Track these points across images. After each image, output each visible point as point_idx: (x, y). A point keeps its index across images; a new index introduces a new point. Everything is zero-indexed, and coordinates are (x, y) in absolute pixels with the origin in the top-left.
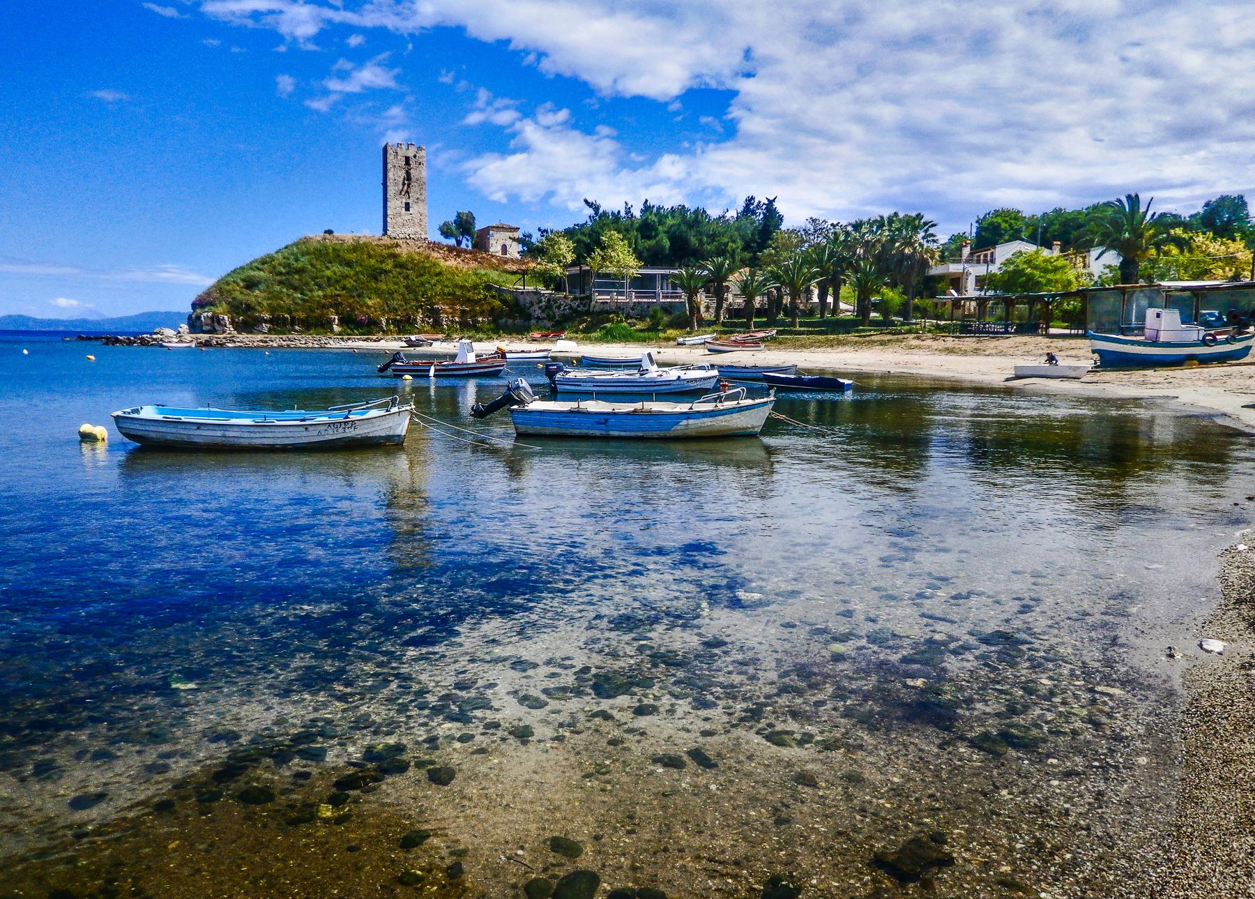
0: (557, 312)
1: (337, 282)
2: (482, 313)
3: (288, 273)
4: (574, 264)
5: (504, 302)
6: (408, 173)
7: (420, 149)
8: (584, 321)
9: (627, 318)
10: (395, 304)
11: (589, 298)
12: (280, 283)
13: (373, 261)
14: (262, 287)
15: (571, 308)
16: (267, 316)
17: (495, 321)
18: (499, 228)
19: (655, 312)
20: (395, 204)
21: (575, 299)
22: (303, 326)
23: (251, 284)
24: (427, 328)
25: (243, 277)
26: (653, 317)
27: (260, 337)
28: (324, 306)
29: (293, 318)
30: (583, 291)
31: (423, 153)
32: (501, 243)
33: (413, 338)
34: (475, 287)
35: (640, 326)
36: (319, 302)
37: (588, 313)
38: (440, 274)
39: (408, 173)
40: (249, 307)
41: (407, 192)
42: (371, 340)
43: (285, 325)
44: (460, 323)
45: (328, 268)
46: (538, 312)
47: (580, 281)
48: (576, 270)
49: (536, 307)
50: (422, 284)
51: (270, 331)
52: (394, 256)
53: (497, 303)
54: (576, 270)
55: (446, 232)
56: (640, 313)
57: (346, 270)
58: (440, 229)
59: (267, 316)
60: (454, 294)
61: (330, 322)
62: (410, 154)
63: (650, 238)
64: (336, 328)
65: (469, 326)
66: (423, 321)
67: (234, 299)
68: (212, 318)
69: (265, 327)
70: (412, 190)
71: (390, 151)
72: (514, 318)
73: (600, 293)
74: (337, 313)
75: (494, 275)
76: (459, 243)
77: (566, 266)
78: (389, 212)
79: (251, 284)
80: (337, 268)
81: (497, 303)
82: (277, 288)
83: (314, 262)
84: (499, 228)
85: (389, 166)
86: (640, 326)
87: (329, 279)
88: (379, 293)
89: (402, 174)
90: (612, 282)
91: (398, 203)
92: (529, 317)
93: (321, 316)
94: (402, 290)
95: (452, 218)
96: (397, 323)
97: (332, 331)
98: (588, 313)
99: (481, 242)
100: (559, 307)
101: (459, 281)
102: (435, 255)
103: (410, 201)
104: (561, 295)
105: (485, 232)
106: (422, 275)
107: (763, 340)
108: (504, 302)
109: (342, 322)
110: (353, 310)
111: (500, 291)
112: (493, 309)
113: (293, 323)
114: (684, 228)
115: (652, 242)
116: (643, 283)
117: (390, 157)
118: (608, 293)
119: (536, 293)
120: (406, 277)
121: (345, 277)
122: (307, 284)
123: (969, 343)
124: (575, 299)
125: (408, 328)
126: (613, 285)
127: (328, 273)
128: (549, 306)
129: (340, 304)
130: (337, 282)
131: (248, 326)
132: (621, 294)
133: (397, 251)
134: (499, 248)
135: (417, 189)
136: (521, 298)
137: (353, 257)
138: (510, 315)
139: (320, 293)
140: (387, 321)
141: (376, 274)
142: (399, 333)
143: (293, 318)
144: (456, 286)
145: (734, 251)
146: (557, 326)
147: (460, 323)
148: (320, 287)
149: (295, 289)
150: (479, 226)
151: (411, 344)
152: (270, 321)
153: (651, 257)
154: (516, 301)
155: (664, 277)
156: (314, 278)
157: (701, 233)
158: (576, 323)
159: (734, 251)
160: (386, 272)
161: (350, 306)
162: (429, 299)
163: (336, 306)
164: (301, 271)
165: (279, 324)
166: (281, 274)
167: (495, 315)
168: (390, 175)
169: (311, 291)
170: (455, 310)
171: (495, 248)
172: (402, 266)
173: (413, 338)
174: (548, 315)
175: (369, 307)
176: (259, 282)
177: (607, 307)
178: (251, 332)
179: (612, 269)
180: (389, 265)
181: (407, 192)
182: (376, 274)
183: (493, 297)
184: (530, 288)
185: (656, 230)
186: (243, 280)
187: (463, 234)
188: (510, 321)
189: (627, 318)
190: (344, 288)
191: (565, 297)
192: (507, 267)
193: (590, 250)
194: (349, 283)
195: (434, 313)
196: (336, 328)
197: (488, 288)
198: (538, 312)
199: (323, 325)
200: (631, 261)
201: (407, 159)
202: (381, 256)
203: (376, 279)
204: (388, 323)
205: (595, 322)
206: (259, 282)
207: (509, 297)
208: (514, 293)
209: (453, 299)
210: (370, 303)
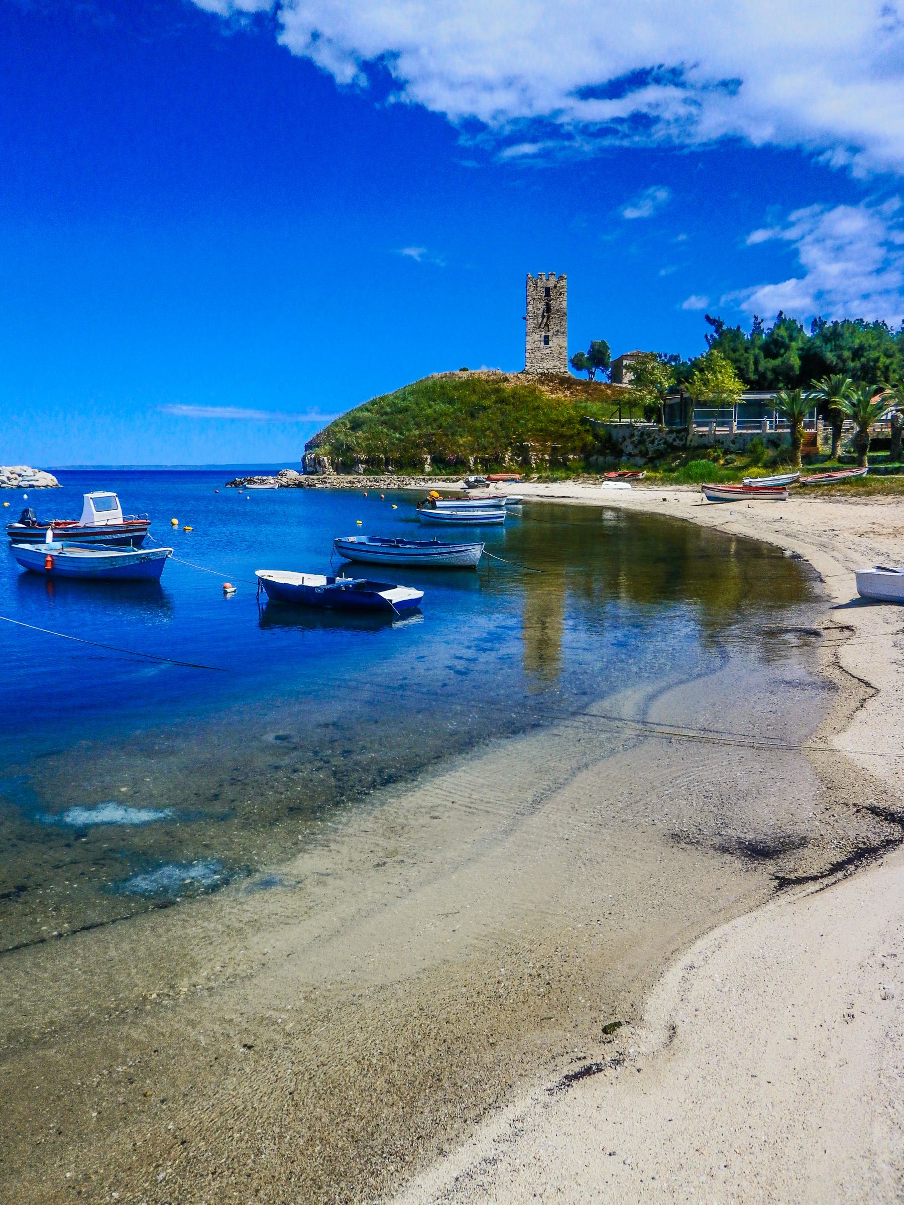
0: (651, 448)
2: (573, 450)
4: (673, 390)
5: (596, 436)
6: (548, 306)
7: (561, 278)
8: (678, 458)
11: (686, 430)
12: (384, 423)
14: (365, 428)
15: (665, 443)
16: (363, 457)
17: (586, 459)
21: (671, 432)
22: (396, 466)
23: (356, 425)
28: (418, 446)
31: (563, 283)
33: (472, 479)
34: (570, 421)
36: (414, 442)
37: (684, 448)
39: (548, 306)
40: (349, 448)
41: (547, 325)
44: (550, 461)
45: (430, 407)
46: (630, 449)
49: (628, 441)
52: (497, 391)
55: (577, 363)
58: (571, 361)
59: (363, 457)
61: (422, 462)
62: (551, 284)
63: (775, 357)
66: (511, 460)
67: (337, 440)
68: (314, 459)
72: (605, 455)
73: (698, 426)
74: (430, 453)
79: (356, 425)
80: (440, 407)
87: (428, 417)
88: (472, 431)
89: (541, 306)
90: (720, 411)
91: (537, 337)
94: (496, 427)
97: (422, 472)
98: (684, 448)
100: (653, 442)
103: (550, 334)
107: (844, 481)
111: (594, 425)
112: (585, 445)
113: (387, 464)
114: (818, 343)
115: (778, 362)
123: (863, 499)
124: (671, 432)
125: (495, 467)
126: (710, 415)
127: (429, 411)
128: (641, 442)
129: (435, 443)
130: (435, 420)
131: (345, 468)
136: (614, 433)
138: (601, 452)
139: (417, 432)
140: (476, 459)
143: (387, 459)
145: (887, 368)
147: (550, 461)
148: (418, 425)
149: (395, 429)
152: (366, 462)
154: (610, 437)
156: (414, 418)
157: (841, 348)
158: (669, 460)
159: (887, 368)
160: (485, 408)
163: (429, 445)
165: (375, 466)
166: (386, 414)
167: (586, 452)
169: (409, 430)
170: (546, 447)
172: (503, 401)
173: (472, 479)
174: (641, 452)
175: (459, 446)
176: (363, 423)
177: (705, 441)
178: (349, 473)
181: (547, 325)
187: (597, 366)
188: (601, 459)
190: (440, 427)
195: (522, 451)
196: (428, 468)
197: (583, 421)
198: (630, 449)
199: (415, 466)
200: (735, 385)
201: (547, 290)
204: (475, 463)
206: (363, 423)
207: (602, 432)
209: (544, 434)
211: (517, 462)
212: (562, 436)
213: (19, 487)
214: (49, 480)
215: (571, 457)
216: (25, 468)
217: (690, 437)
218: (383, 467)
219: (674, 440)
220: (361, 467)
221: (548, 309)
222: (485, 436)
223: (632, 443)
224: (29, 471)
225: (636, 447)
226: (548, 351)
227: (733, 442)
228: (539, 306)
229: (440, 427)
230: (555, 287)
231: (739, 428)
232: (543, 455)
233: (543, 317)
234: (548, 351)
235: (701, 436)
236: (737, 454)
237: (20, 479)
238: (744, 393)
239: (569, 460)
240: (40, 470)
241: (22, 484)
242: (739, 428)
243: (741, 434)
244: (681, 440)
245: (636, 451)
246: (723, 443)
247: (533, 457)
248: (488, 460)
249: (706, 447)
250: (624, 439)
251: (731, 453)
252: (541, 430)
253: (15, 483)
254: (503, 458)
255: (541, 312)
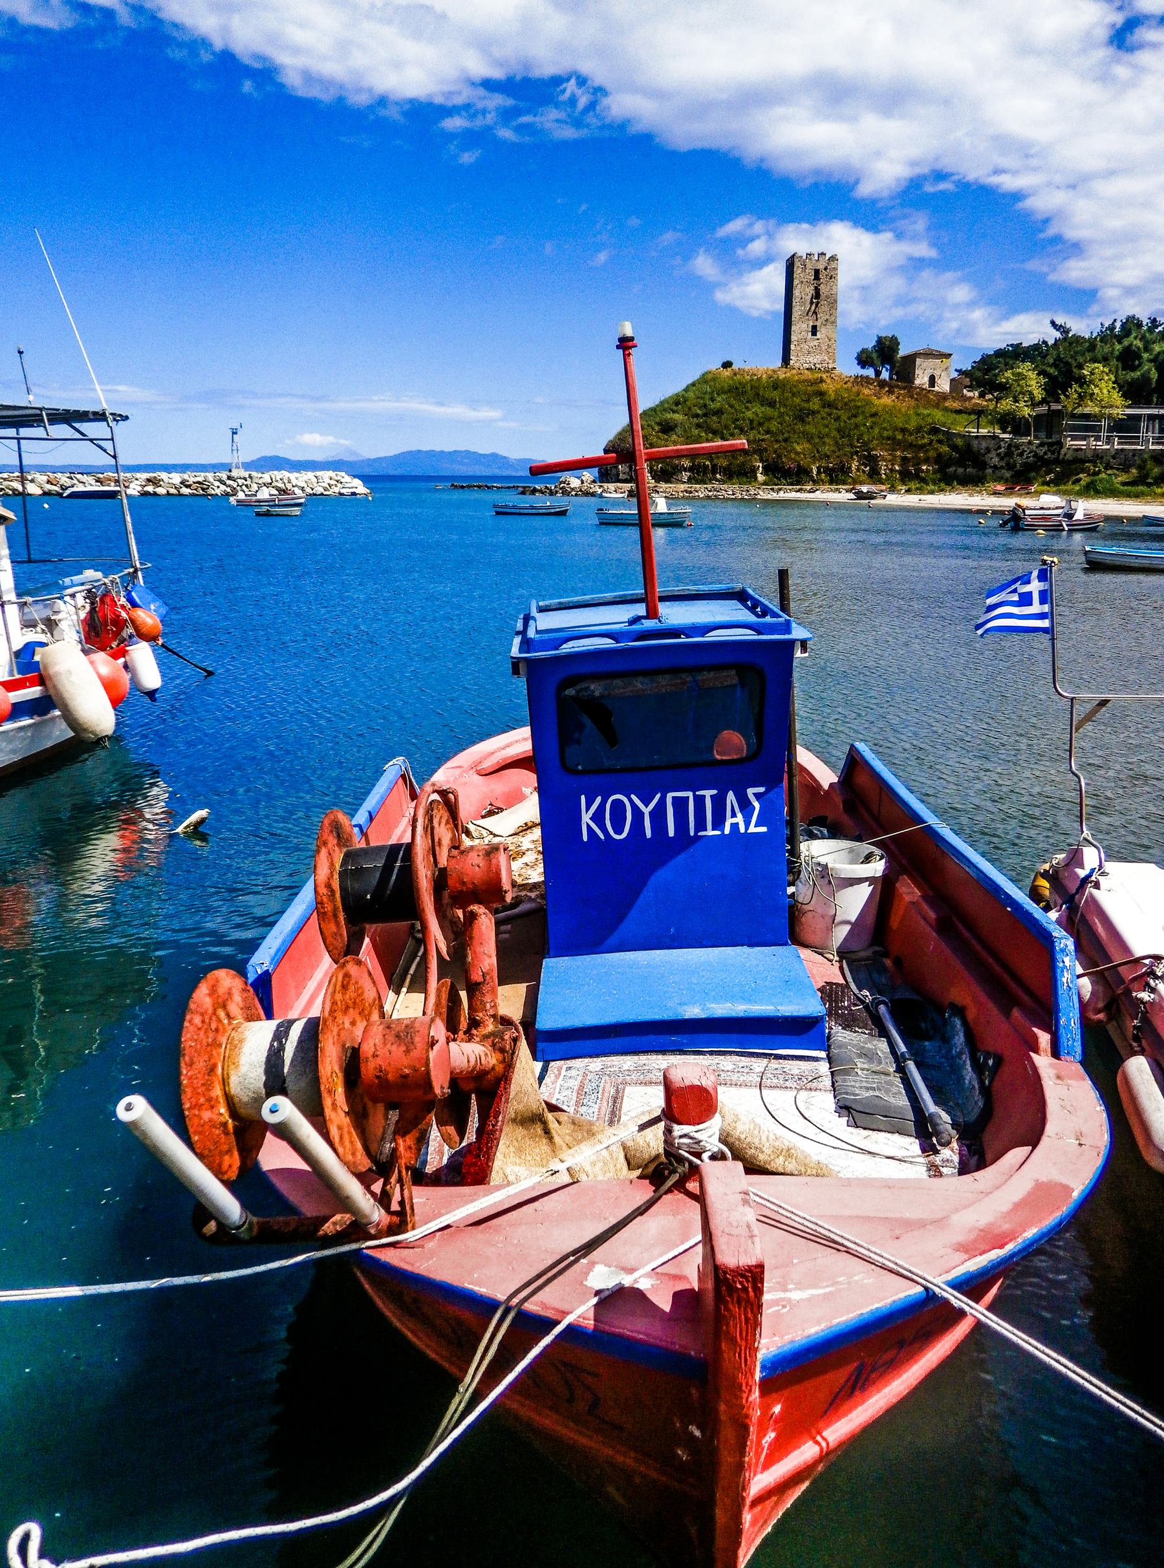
1: (760, 424)
2: (927, 461)
3: (705, 415)
4: (1044, 401)
5: (954, 447)
6: (817, 290)
9: (1106, 468)
10: (826, 449)
11: (1060, 444)
12: (698, 426)
13: (797, 400)
14: (679, 430)
15: (1036, 455)
18: (929, 354)
19: (1144, 461)
20: (800, 328)
21: (1042, 445)
24: (864, 477)
25: (658, 420)
26: (1140, 468)
27: (682, 487)
29: (714, 466)
30: (1049, 436)
32: (929, 372)
34: (919, 429)
35: (1123, 478)
37: (1057, 461)
38: (874, 415)
39: (817, 290)
41: (815, 313)
42: (805, 491)
43: (705, 473)
44: (900, 472)
46: (996, 460)
47: (1049, 423)
48: (1044, 409)
49: (993, 454)
50: (857, 426)
51: (690, 480)
52: (821, 394)
53: (945, 449)
54: (1044, 409)
56: (1124, 462)
57: (769, 411)
60: (893, 439)
61: (754, 470)
63: (1134, 369)
64: (761, 478)
65: (910, 477)
66: (858, 470)
69: (685, 476)
70: (821, 310)
71: (797, 264)
72: (965, 467)
73: (1074, 438)
74: (761, 461)
75: (938, 415)
76: (878, 373)
77: (1034, 405)
78: (793, 338)
81: (945, 449)
82: (696, 432)
83: (733, 401)
84: (929, 354)
85: (796, 282)
86: (1123, 478)
87: (751, 421)
88: (809, 438)
89: (810, 291)
90: (1088, 425)
92: (983, 466)
93: (743, 464)
94: (834, 433)
95: (870, 344)
96: (827, 471)
97: (756, 479)
98: (1057, 461)
99: (905, 370)
100: (1021, 455)
101: (899, 422)
102: (866, 391)
103: (818, 324)
104: (1025, 440)
105: (911, 359)
106: (855, 416)
108: (954, 447)
109: (766, 471)
110: (779, 457)
112: (939, 455)
116: (1126, 427)
117: (798, 271)
118: (1084, 438)
119: (994, 437)
120: (838, 419)
121: (770, 419)
122: (727, 427)
127: (749, 414)
128: (1009, 454)
129: (766, 450)
130: (760, 424)
132: (1098, 439)
133: (824, 386)
134: (926, 379)
135: (826, 308)
136: (975, 443)
137: (776, 395)
138: (960, 463)
141: (802, 416)
142: (831, 483)
143: (714, 466)
144: (896, 429)
146: (1021, 477)
147: (900, 472)
150: (903, 352)
151: (860, 496)
152: (691, 469)
153: (1134, 392)
154: (968, 446)
155: (1151, 418)
160: (814, 413)
161: (775, 452)
162: (865, 444)
163: (760, 452)
164: (719, 412)
166: (697, 416)
167: (942, 463)
168: (796, 293)
171: (921, 380)
172: (830, 405)
174: (1008, 464)
175: (798, 454)
177: (1080, 455)
179: (1090, 408)
180: (815, 404)
181: (815, 313)
182: (802, 416)
183: (940, 442)
184: (983, 431)
185: (1140, 357)
186: (658, 424)
188: (960, 470)
189: (1106, 468)
191: (1030, 443)
192: (947, 404)
193: (1065, 387)
194: (774, 426)
195: (871, 461)
196: (761, 478)
197: (934, 431)
198: (996, 460)
200: (1117, 397)
201: (817, 272)
202: (805, 393)
203: (803, 421)
204: (819, 473)
205: (1064, 472)
206: (676, 426)
207: (959, 442)
208: (967, 438)
209: (894, 444)
210: (798, 448)
211: (864, 472)
212: (911, 445)
213: (341, 494)
214: (360, 488)
215: (924, 468)
216: (343, 474)
217: (1063, 451)
218: (710, 476)
219: (1045, 453)
220: (685, 476)
221: (817, 294)
222: (824, 443)
223: (998, 455)
224: (347, 479)
225: (1002, 459)
226: (816, 343)
227: (1114, 457)
228: (807, 290)
229: (767, 432)
230: (826, 269)
231: (1119, 443)
232: (893, 465)
233: (812, 303)
234: (816, 343)
235: (1077, 450)
236: (1118, 469)
237: (339, 485)
238: (1128, 407)
239: (922, 471)
240: (355, 476)
241: (343, 491)
242: (1119, 443)
243: (1122, 450)
244: (1053, 453)
245: (1003, 464)
246: (1102, 458)
247: (883, 468)
248: (833, 470)
249: (1083, 461)
250: (988, 450)
251: (1112, 468)
252: (888, 438)
253: (336, 490)
254: (850, 468)
255: (809, 297)
